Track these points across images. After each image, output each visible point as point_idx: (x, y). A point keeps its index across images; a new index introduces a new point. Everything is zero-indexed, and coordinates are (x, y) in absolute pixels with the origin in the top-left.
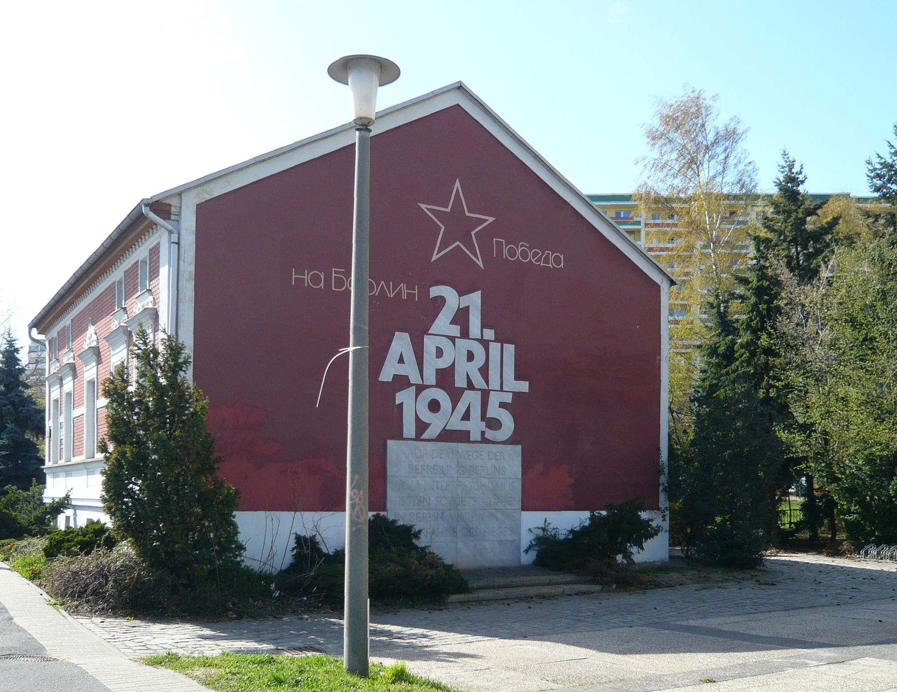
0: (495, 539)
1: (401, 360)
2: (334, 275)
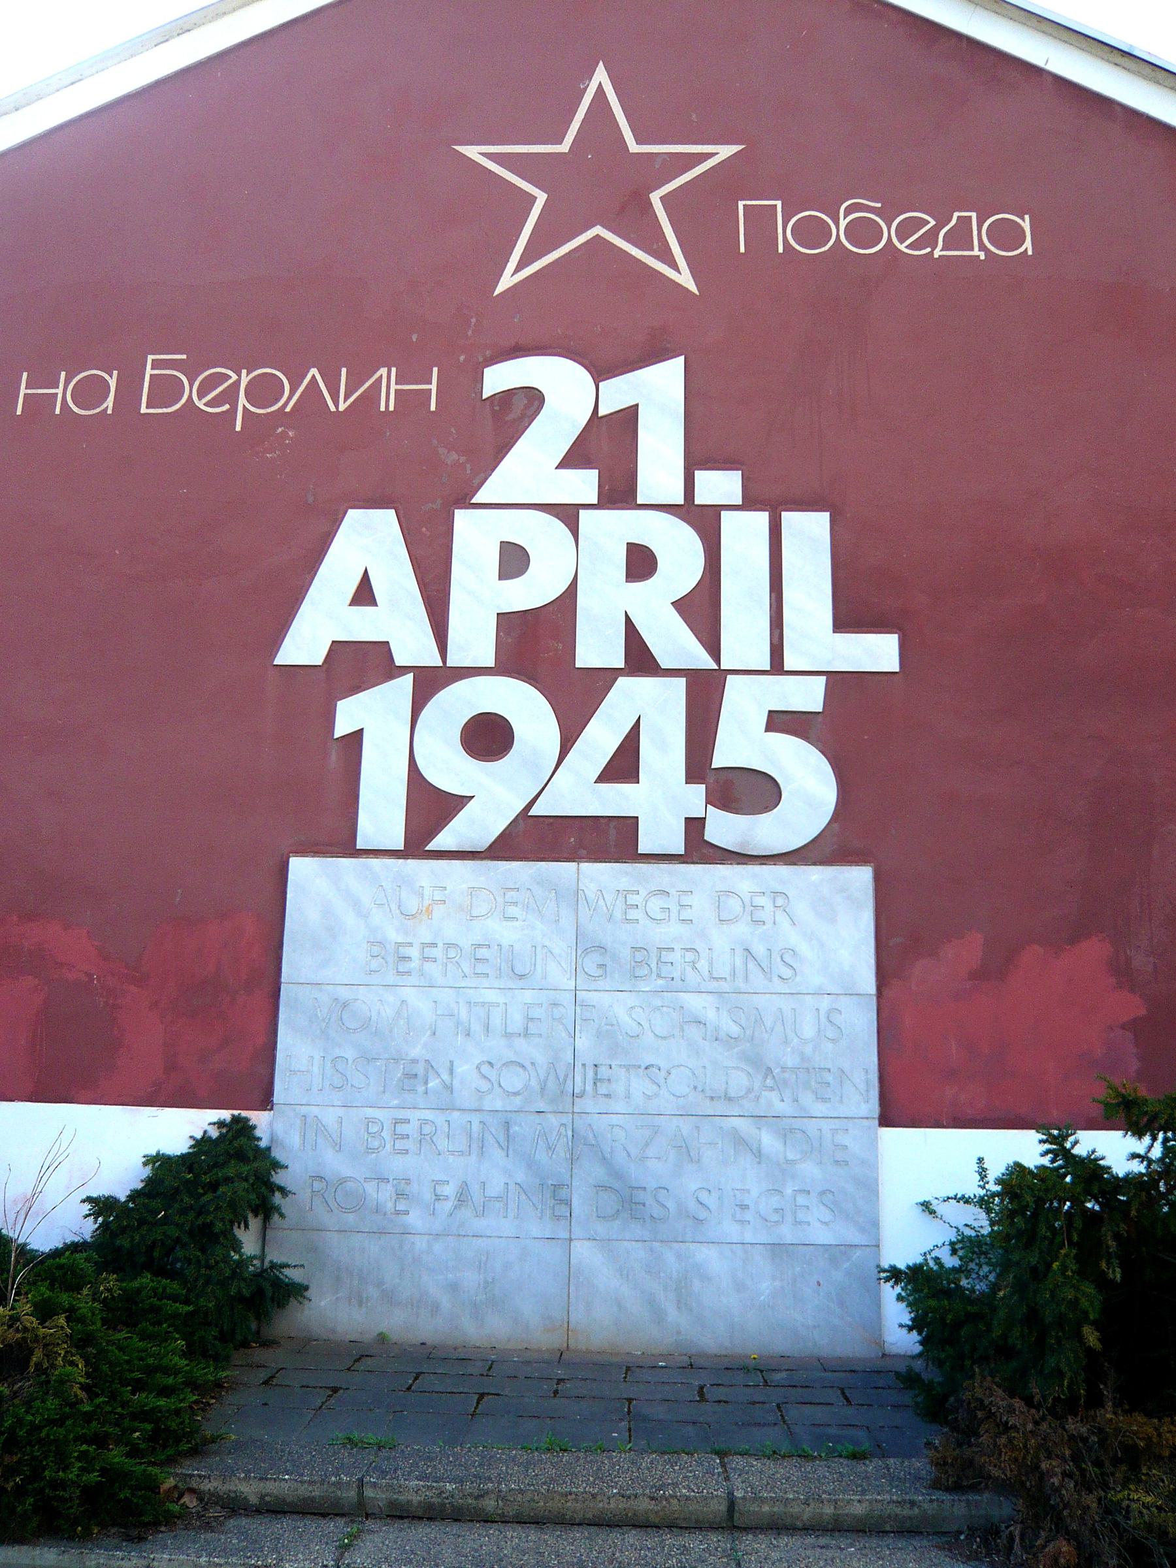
0: (749, 1238)
1: (364, 595)
2: (149, 371)
